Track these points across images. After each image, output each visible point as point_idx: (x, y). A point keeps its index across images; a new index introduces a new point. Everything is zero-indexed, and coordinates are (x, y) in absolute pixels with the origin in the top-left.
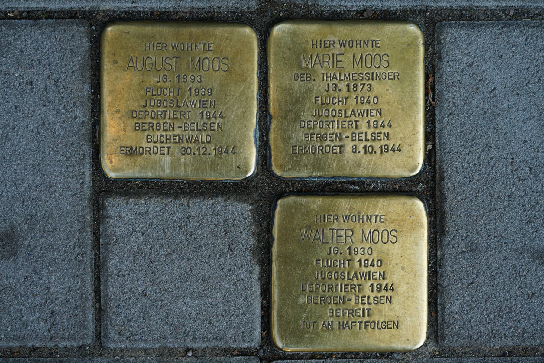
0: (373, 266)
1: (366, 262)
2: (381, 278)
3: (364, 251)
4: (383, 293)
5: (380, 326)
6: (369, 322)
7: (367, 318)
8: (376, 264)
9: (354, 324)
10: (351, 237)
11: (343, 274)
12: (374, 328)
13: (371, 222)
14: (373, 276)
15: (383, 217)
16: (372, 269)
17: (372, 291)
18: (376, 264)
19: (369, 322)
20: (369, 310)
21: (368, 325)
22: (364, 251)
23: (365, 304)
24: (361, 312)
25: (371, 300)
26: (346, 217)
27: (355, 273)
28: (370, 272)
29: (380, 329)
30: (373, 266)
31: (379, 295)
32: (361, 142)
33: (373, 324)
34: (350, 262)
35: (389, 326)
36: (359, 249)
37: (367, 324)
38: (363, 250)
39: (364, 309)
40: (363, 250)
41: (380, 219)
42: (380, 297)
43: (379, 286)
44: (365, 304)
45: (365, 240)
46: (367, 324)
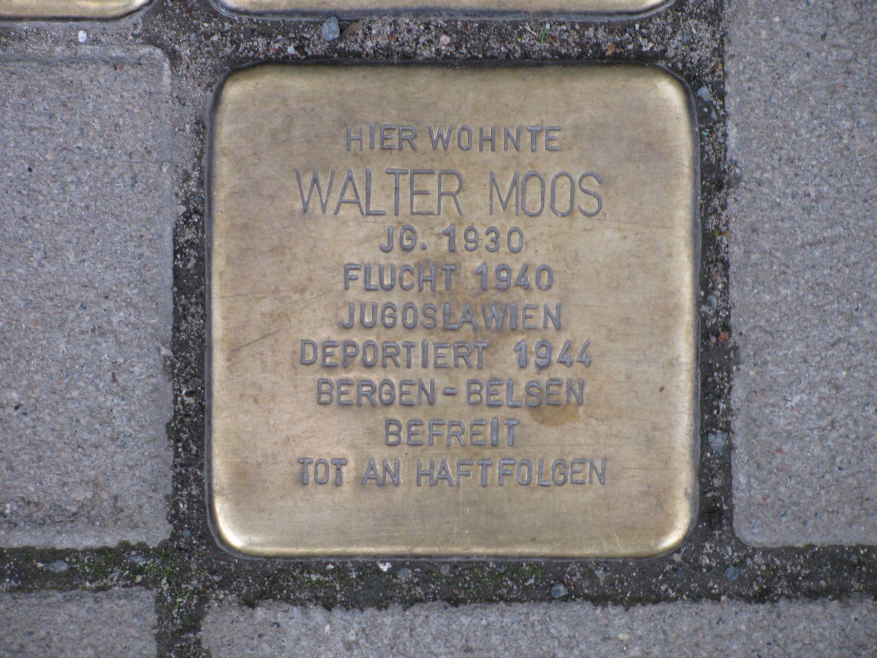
40: (493, 235)
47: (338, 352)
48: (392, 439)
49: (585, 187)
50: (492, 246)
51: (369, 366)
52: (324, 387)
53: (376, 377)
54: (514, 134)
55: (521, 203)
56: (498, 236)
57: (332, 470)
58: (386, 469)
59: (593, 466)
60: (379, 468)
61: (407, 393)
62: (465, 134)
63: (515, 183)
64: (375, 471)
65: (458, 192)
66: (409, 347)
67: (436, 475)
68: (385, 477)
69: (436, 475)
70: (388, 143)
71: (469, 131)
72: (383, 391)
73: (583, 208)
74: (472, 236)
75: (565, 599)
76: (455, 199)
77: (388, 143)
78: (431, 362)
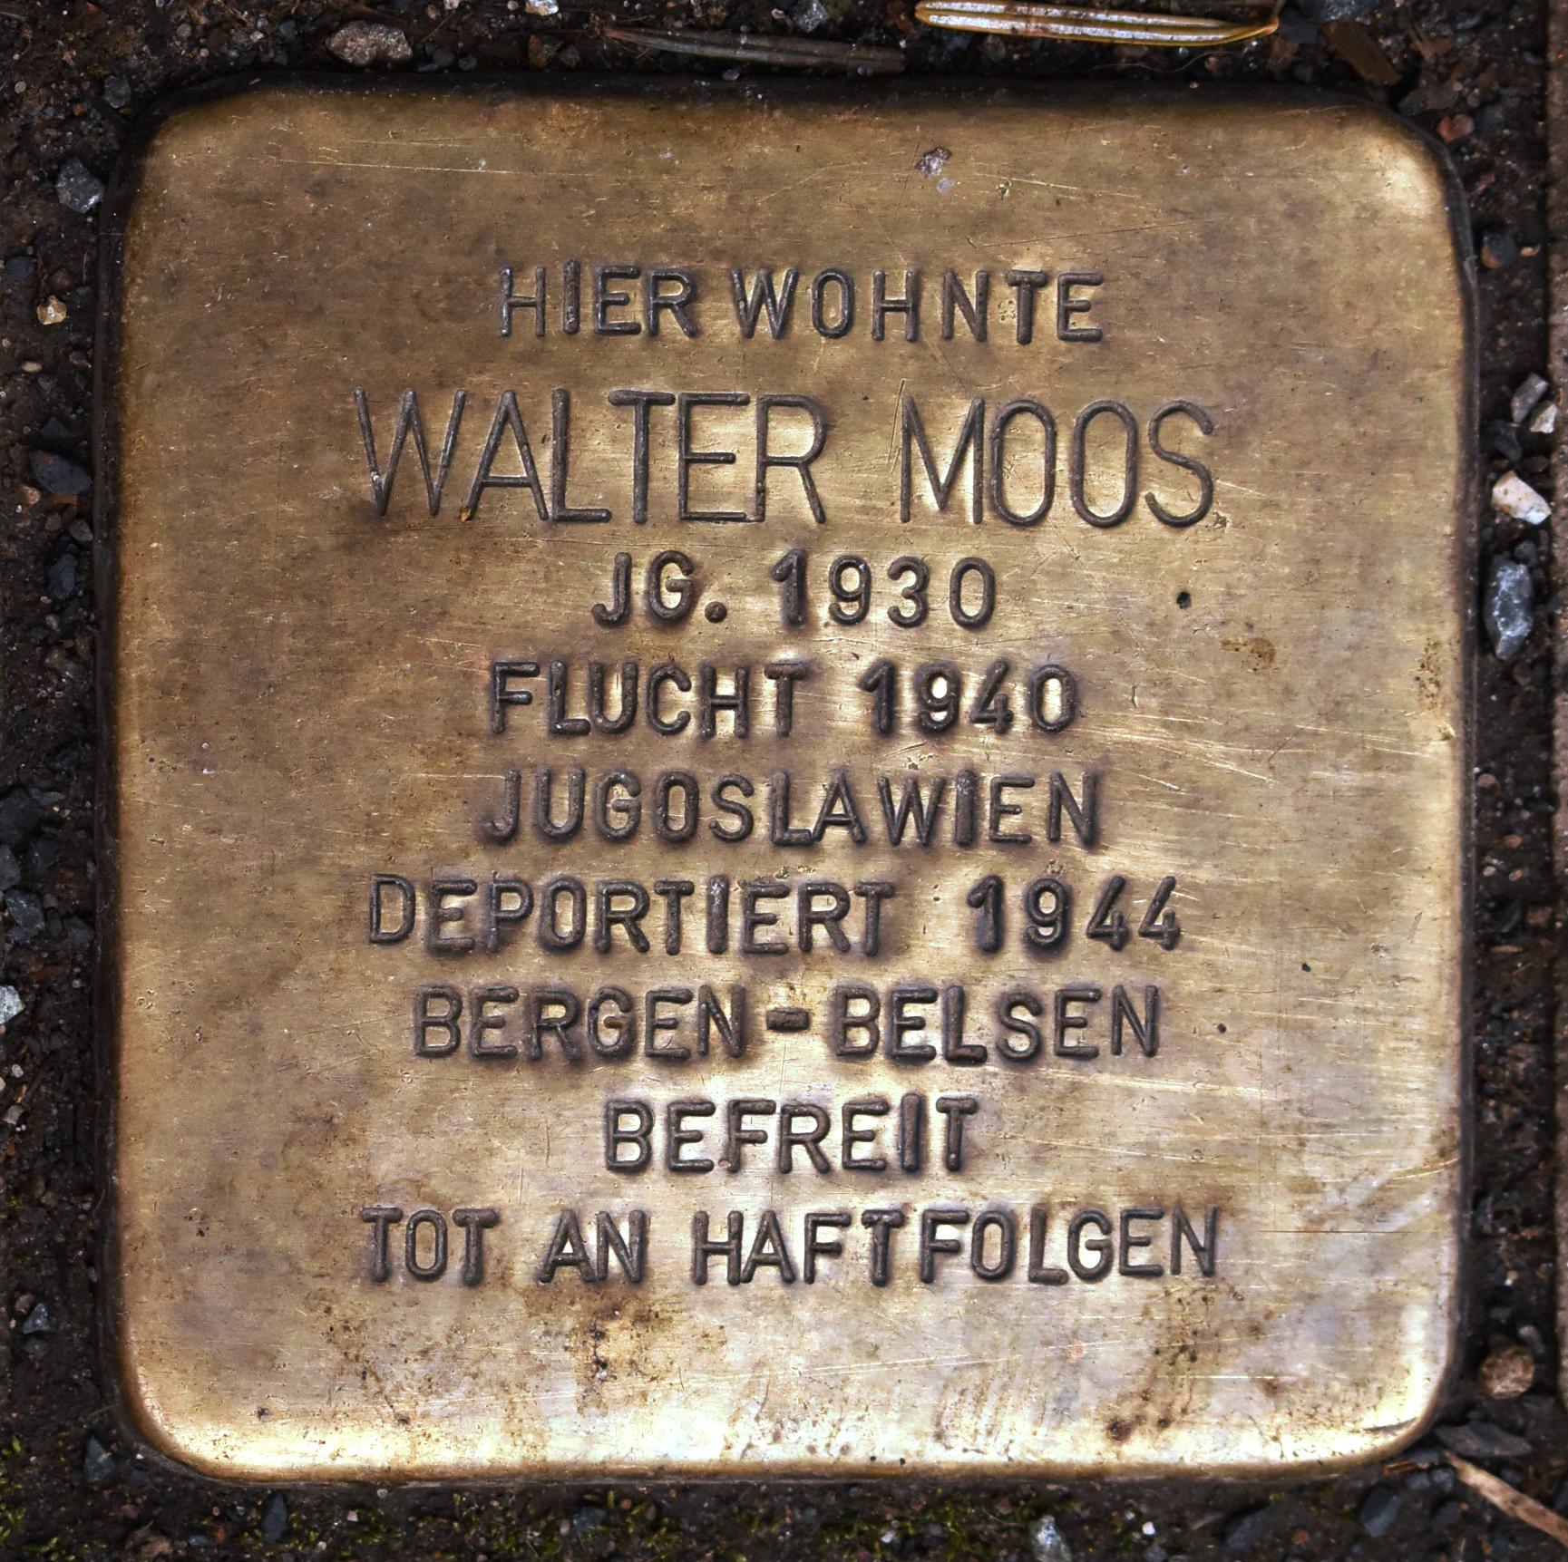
0: (1003, 724)
1: (940, 689)
2: (1069, 833)
3: (918, 594)
4: (1088, 964)
5: (1056, 1255)
6: (959, 1219)
7: (941, 1191)
8: (1019, 703)
9: (826, 1235)
10: (805, 465)
11: (734, 795)
12: (1004, 1272)
13: (982, 336)
14: (1001, 811)
15: (1085, 294)
16: (980, 749)
17: (991, 946)
18: (1019, 703)
19: (959, 1219)
20: (960, 1112)
21: (954, 1249)
22: (918, 594)
23: (921, 1057)
24: (889, 1126)
25: (980, 1027)
26: (912, 801)
27: (842, 788)
28: (972, 777)
29: (1058, 1279)
30: (1003, 724)
31: (1050, 981)
32: (1053, 1291)
33: (994, 1233)
34: (888, 907)
35: (1139, 1257)
36: (880, 571)
37: (945, 1233)
38: (910, 579)
39: (915, 1111)
40: (910, 579)
41: (1065, 313)
42: (1065, 998)
43: (1048, 904)
44: (921, 1057)
45: (929, 498)
46: (945, 1233)
47: (714, 1127)
48: (631, 1153)
49: (1167, 445)
50: (909, 608)
51: (562, 949)
52: (440, 1009)
53: (587, 977)
54: (971, 288)
55: (992, 495)
56: (923, 582)
57: (458, 1240)
58: (609, 1237)
59: (1182, 1226)
60: (591, 1237)
61: (870, 1136)
62: (426, 1260)
63: (973, 429)
64: (580, 1244)
65: (817, 454)
66: (678, 893)
67: (746, 1252)
68: (604, 1260)
69: (746, 1252)
70: (616, 318)
71: (819, 323)
72: (603, 1018)
73: (1161, 499)
74: (852, 581)
75: (90, 441)
76: (807, 476)
77: (616, 318)
78: (735, 942)
